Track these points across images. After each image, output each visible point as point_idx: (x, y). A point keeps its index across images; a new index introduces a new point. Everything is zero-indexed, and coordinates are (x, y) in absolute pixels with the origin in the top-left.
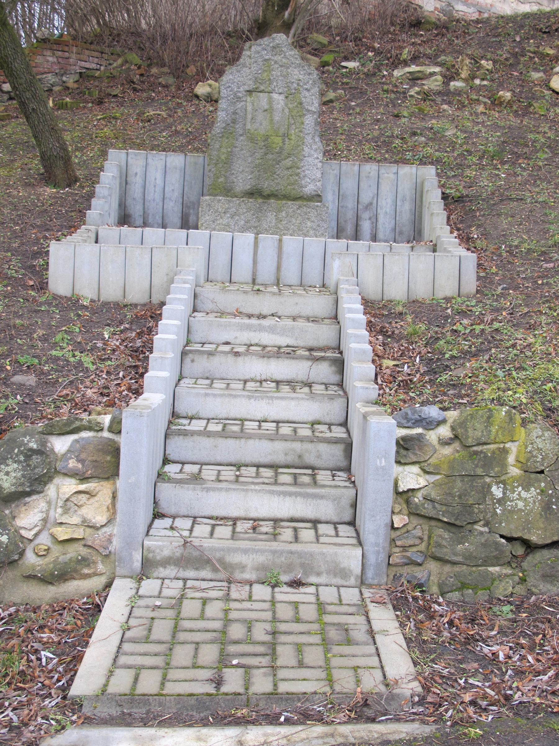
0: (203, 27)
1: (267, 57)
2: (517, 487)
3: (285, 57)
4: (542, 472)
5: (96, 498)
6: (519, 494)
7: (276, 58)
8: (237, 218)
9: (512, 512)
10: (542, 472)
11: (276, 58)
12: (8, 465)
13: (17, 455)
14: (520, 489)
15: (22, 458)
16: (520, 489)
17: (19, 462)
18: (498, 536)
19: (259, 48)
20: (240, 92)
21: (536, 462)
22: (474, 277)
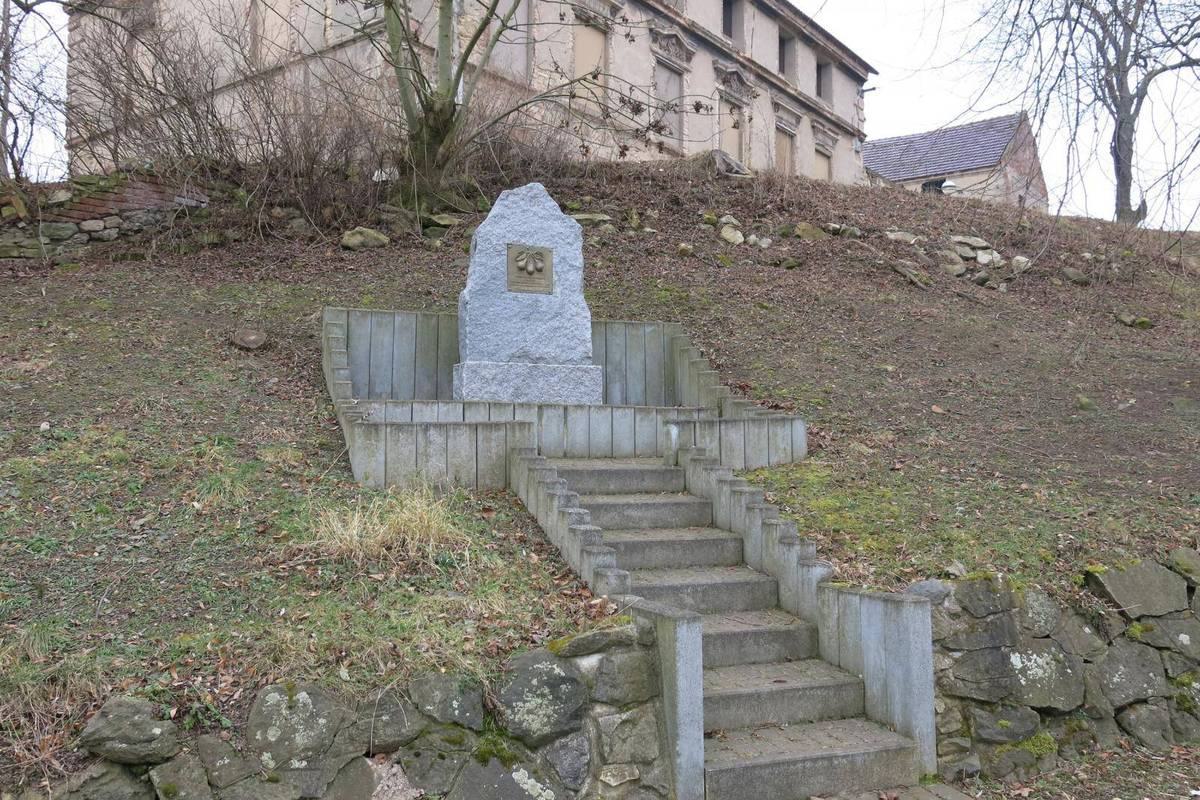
0: (347, 141)
1: (525, 208)
2: (1032, 655)
3: (544, 208)
4: (1048, 636)
5: (931, 643)
6: (1036, 662)
7: (534, 209)
8: (506, 384)
9: (1034, 681)
10: (1048, 636)
11: (534, 209)
12: (525, 702)
13: (538, 687)
14: (1035, 656)
15: (546, 691)
16: (1035, 656)
17: (543, 696)
18: (1029, 708)
19: (516, 198)
20: (500, 245)
21: (1040, 627)
22: (805, 445)
